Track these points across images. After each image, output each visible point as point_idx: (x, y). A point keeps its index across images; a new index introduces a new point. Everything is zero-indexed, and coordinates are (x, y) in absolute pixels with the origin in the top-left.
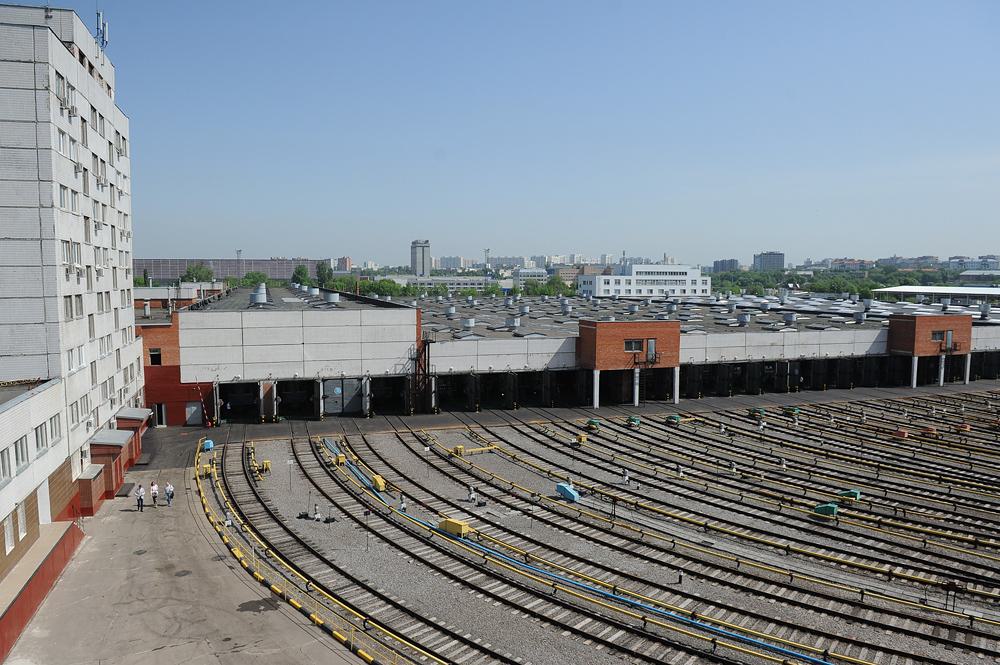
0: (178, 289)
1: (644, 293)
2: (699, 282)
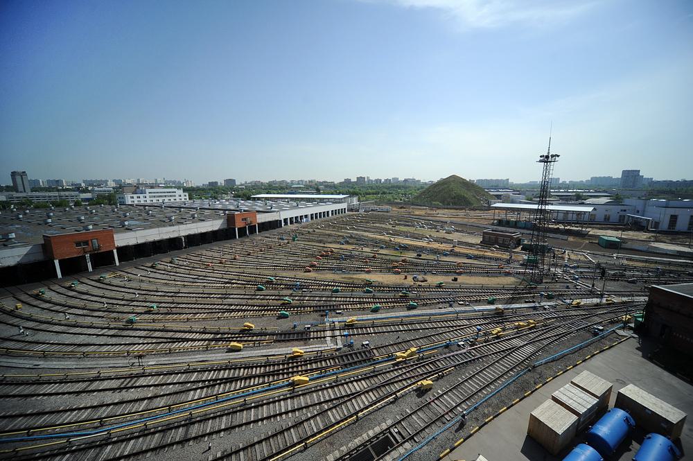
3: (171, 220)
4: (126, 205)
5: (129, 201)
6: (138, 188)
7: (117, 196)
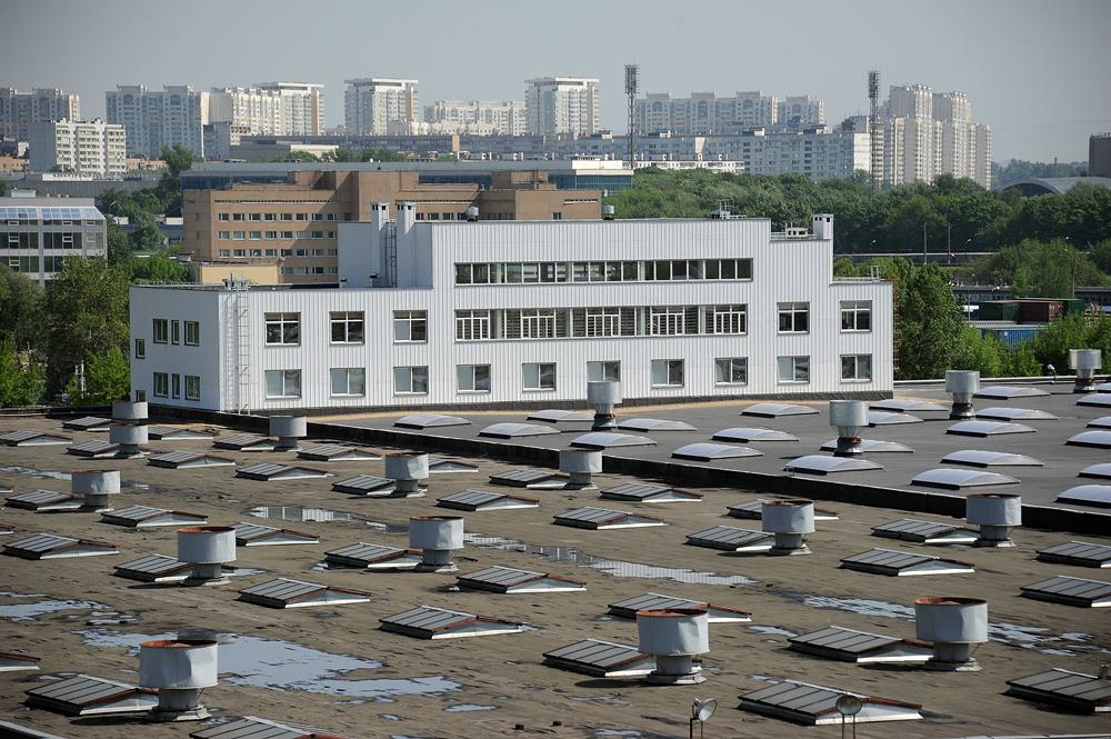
0: (1028, 261)
1: (508, 386)
2: (826, 317)
3: (669, 670)
4: (209, 416)
5: (245, 377)
6: (346, 203)
7: (147, 304)
